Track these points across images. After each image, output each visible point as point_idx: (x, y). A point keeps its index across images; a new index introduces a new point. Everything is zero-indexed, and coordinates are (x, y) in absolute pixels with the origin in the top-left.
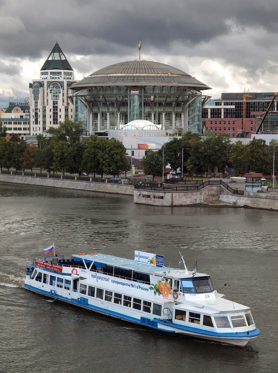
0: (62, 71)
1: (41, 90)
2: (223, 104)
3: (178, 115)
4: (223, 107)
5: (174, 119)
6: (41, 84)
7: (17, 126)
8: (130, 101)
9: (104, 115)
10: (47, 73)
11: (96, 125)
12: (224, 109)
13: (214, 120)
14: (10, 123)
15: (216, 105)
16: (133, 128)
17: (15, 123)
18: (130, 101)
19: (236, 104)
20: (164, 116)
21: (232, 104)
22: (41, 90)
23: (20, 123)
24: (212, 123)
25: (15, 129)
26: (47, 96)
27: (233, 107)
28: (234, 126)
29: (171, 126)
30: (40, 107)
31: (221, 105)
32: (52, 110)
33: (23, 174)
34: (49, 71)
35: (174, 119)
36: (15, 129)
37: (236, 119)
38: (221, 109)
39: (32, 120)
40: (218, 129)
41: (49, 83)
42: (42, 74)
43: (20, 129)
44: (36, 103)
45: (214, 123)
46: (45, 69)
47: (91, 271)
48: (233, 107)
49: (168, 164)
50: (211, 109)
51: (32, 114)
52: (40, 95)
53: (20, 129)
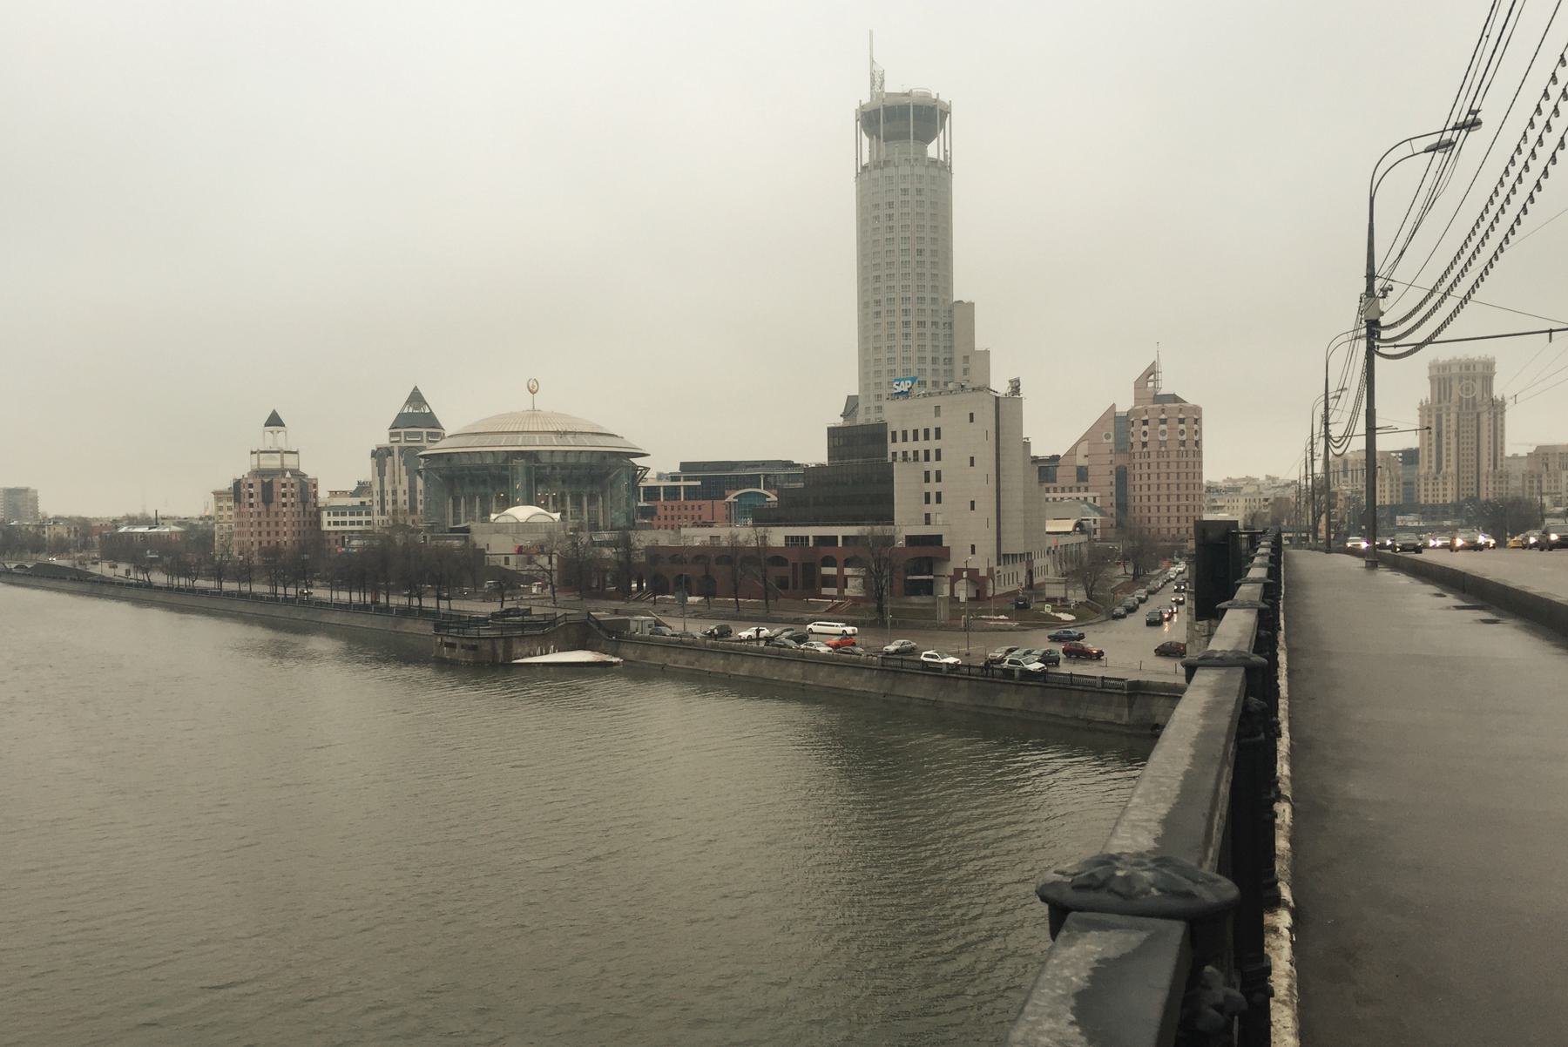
0: (425, 431)
1: (389, 460)
2: (682, 479)
3: (592, 499)
4: (682, 483)
5: (585, 504)
6: (389, 452)
7: (356, 518)
8: (512, 476)
9: (470, 502)
10: (398, 434)
11: (456, 514)
12: (684, 486)
13: (669, 504)
14: (344, 514)
15: (672, 481)
16: (511, 520)
17: (352, 514)
18: (512, 476)
19: (702, 479)
20: (568, 498)
21: (695, 479)
22: (389, 460)
23: (359, 514)
24: (666, 509)
25: (352, 523)
26: (400, 469)
27: (699, 483)
28: (700, 512)
29: (582, 514)
30: (388, 488)
31: (680, 480)
32: (407, 492)
33: (840, 539)
34: (402, 431)
35: (585, 504)
36: (352, 523)
37: (703, 502)
38: (679, 486)
39: (377, 508)
40: (669, 518)
41: (402, 450)
42: (392, 435)
43: (344, 523)
44: (382, 482)
45: (669, 508)
46: (396, 428)
47: (1149, 629)
48: (699, 483)
49: (901, 543)
50: (664, 487)
51: (377, 498)
52: (388, 470)
53: (344, 523)
